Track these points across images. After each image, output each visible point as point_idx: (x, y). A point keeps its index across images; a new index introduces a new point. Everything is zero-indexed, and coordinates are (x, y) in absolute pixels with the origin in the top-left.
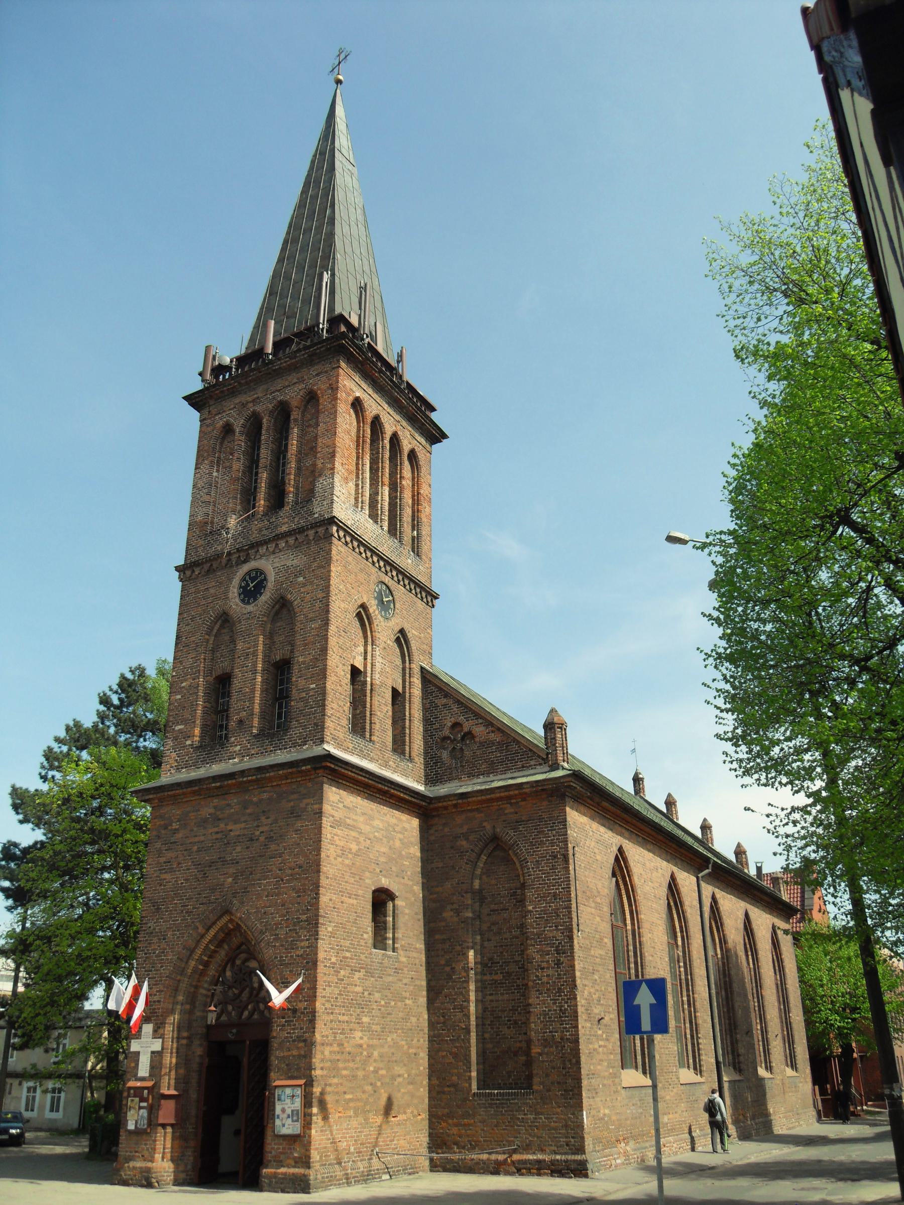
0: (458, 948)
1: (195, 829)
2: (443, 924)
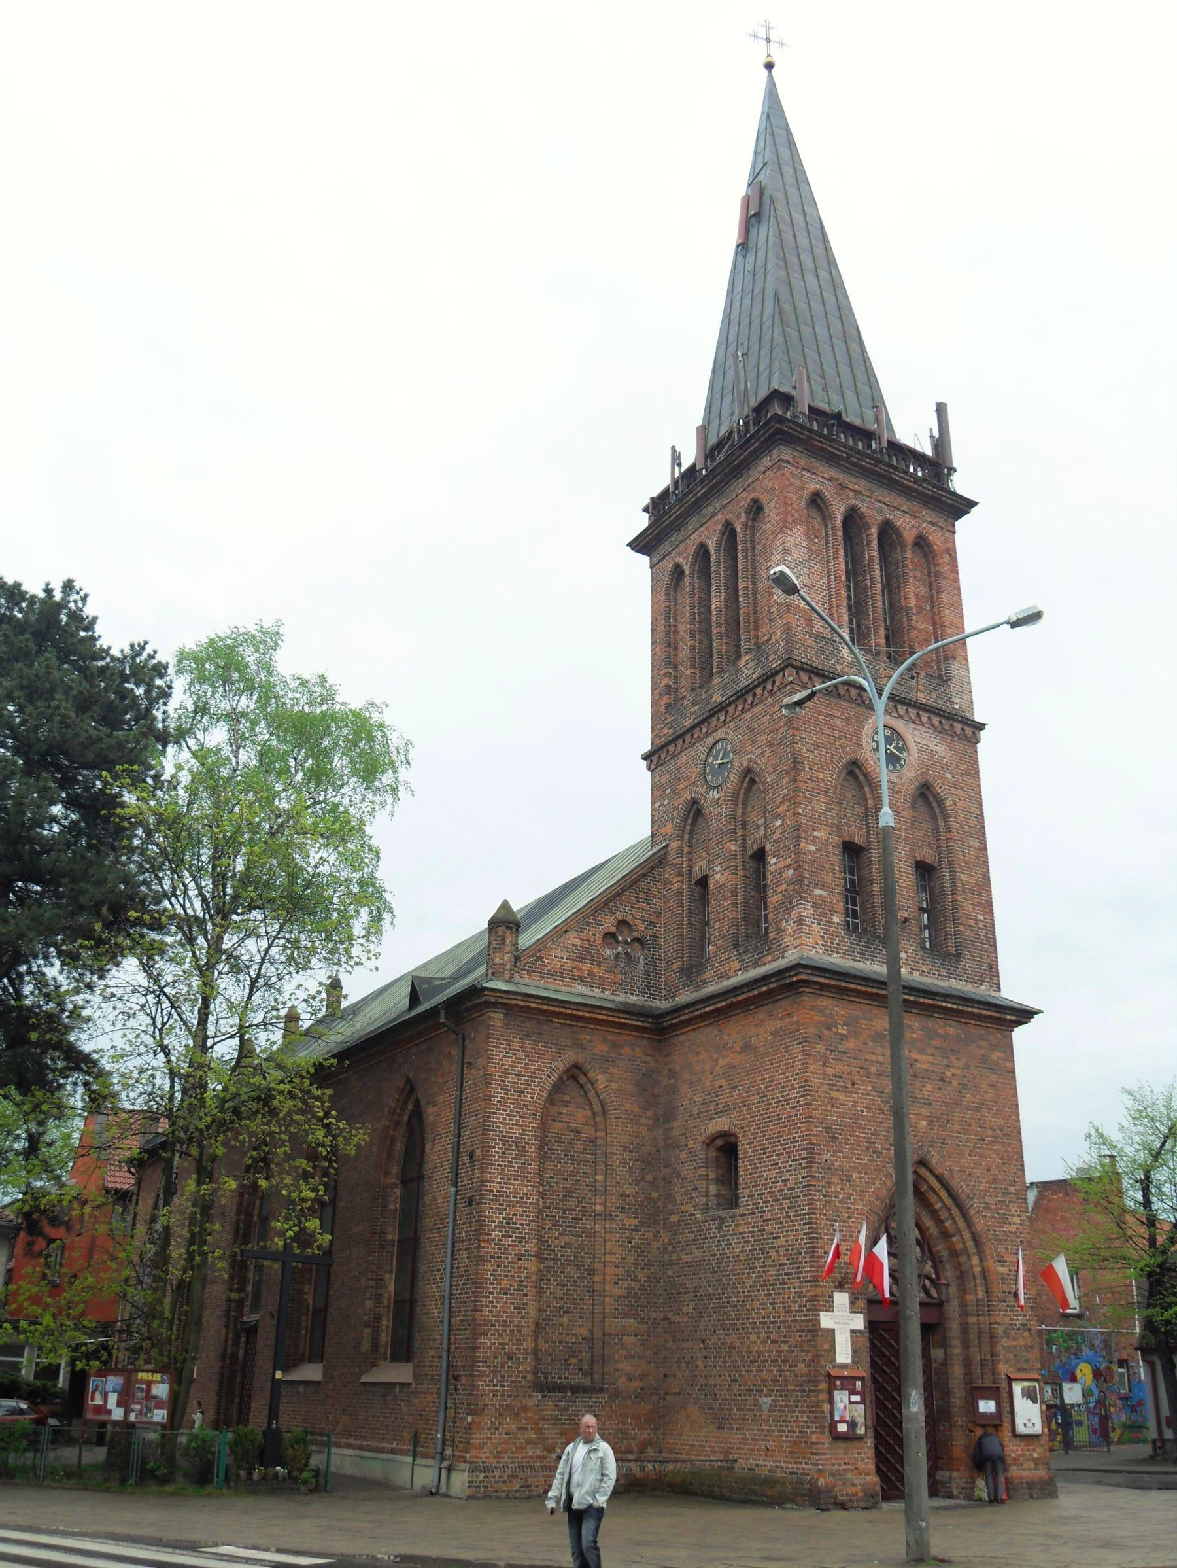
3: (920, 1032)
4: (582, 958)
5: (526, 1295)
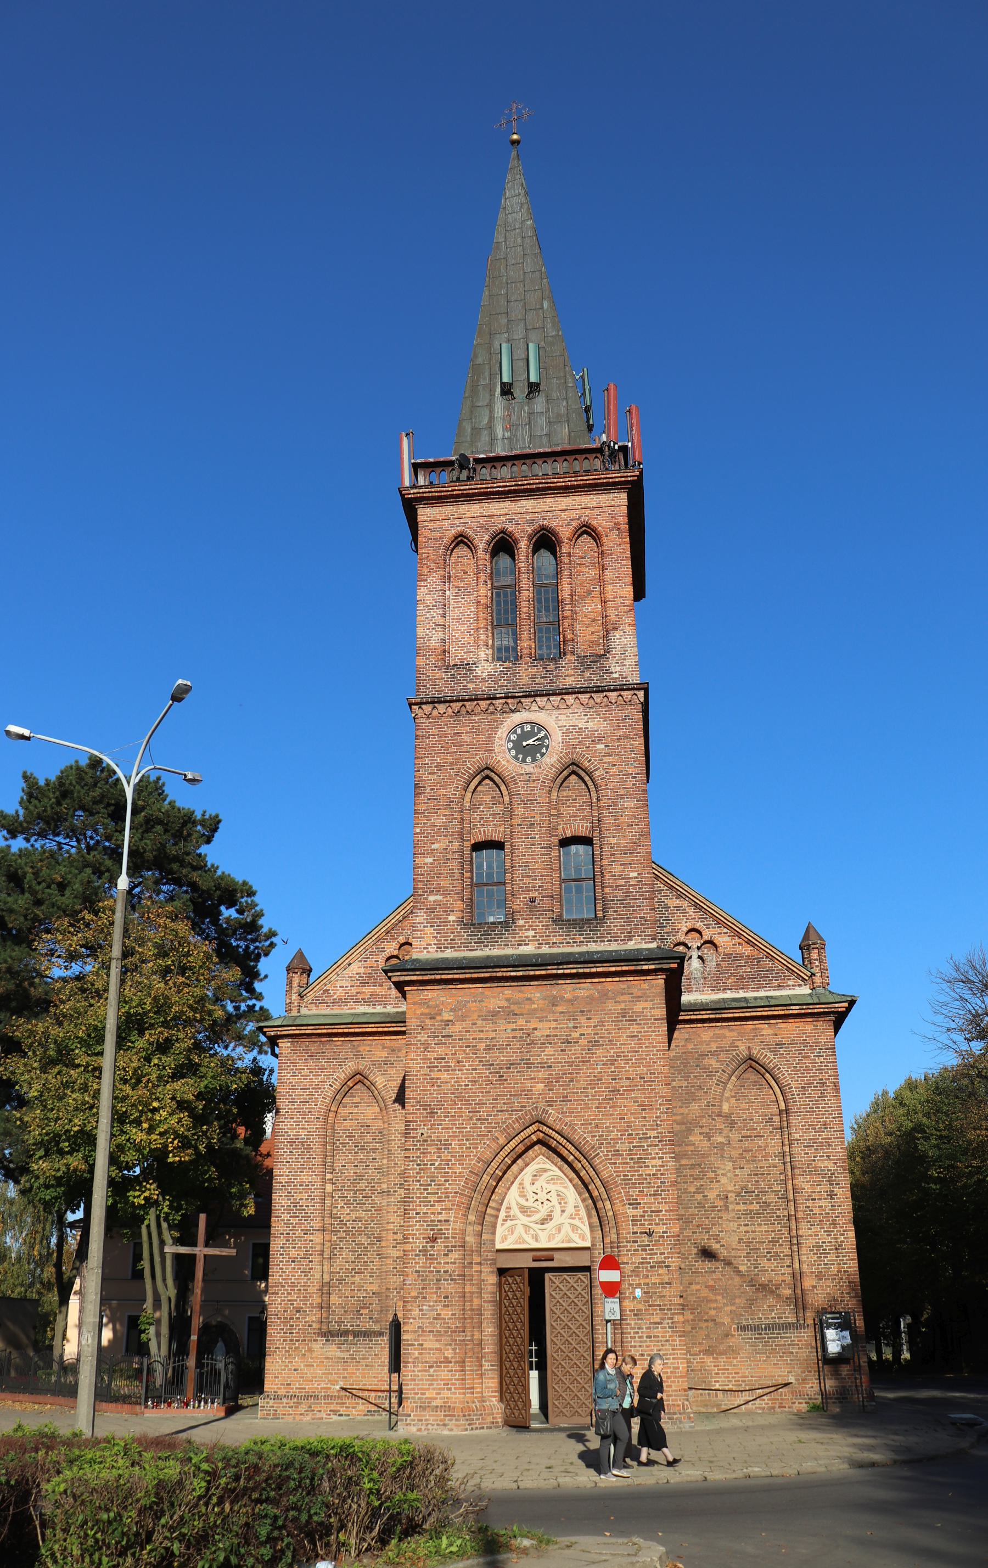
0: (712, 1175)
1: (479, 1023)
2: (692, 1148)
3: (540, 1002)
4: (365, 983)
5: (311, 1261)
